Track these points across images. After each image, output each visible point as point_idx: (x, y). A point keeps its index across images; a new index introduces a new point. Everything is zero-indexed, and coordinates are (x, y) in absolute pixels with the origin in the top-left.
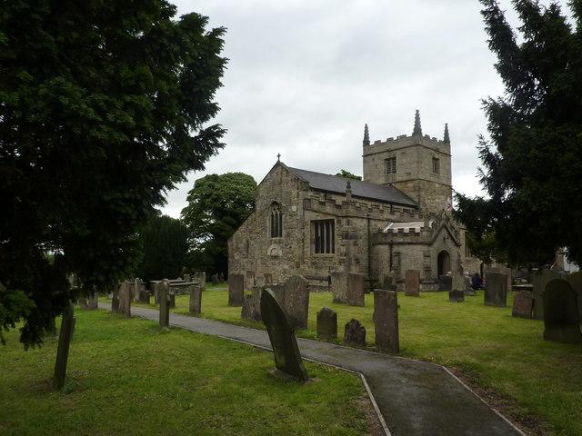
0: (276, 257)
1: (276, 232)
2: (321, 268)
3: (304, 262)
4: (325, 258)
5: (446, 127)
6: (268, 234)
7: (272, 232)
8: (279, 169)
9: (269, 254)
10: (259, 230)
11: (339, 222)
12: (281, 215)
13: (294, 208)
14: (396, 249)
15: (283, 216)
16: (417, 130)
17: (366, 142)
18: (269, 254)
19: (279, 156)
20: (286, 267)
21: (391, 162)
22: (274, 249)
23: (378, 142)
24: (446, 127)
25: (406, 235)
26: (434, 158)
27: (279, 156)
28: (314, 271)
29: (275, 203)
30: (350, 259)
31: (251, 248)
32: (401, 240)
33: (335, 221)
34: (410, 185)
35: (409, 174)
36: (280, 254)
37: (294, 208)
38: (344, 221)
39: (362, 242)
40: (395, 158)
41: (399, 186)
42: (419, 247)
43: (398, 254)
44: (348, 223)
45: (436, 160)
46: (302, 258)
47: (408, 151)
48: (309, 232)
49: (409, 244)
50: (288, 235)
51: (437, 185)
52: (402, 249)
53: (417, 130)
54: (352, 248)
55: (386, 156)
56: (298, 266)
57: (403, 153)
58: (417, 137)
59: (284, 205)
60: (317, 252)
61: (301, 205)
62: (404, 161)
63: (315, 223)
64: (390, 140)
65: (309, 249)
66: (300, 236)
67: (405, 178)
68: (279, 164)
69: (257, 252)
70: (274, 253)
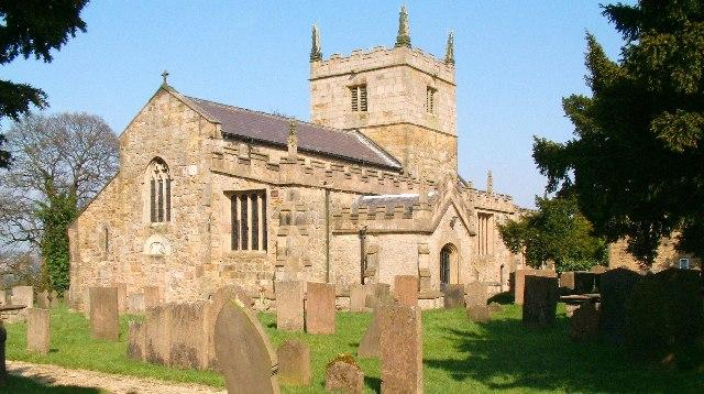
1: (159, 212)
2: (243, 276)
11: (274, 194)
12: (169, 181)
13: (193, 170)
18: (146, 252)
20: (180, 276)
22: (153, 245)
29: (160, 161)
31: (113, 243)
36: (168, 250)
38: (284, 192)
40: (364, 86)
46: (208, 260)
48: (224, 211)
55: (347, 81)
56: (200, 272)
57: (380, 78)
60: (235, 247)
69: (125, 250)
70: (156, 250)
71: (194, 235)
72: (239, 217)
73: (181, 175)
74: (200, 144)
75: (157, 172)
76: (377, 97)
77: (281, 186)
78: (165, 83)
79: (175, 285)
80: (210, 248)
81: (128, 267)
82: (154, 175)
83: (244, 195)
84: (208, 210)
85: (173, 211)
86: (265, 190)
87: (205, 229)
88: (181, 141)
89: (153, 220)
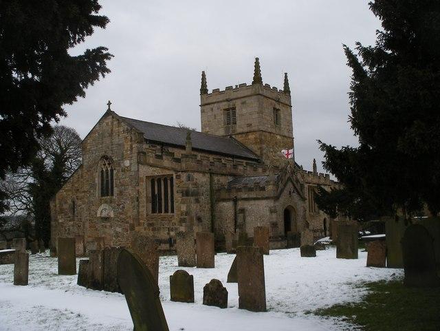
0: (106, 219)
1: (107, 190)
2: (159, 229)
3: (139, 225)
4: (163, 219)
5: (286, 77)
6: (98, 193)
8: (109, 120)
9: (99, 212)
10: (86, 188)
11: (178, 177)
13: (127, 163)
14: (240, 205)
15: (115, 172)
16: (257, 78)
17: (204, 90)
19: (109, 104)
20: (119, 230)
21: (230, 113)
22: (104, 210)
23: (216, 91)
24: (286, 77)
26: (274, 109)
27: (109, 104)
28: (151, 233)
30: (191, 219)
31: (78, 210)
32: (246, 196)
33: (174, 177)
34: (251, 137)
35: (249, 125)
37: (127, 163)
38: (184, 176)
39: (204, 199)
40: (234, 109)
41: (239, 138)
42: (264, 202)
43: (243, 211)
44: (189, 178)
45: (276, 110)
46: (137, 219)
47: (248, 100)
48: (144, 190)
49: (255, 199)
50: (121, 193)
51: (278, 137)
53: (257, 78)
54: (194, 206)
55: (225, 105)
56: (132, 228)
57: (243, 103)
58: (257, 86)
60: (154, 211)
61: (135, 159)
62: (244, 111)
63: (153, 180)
64: (229, 88)
65: (145, 208)
66: (134, 194)
67: (246, 130)
68: (109, 113)
70: (104, 214)
72: (105, 182)
73: (119, 165)
74: (131, 146)
75: (105, 165)
76: (242, 115)
78: (109, 110)
79: (117, 235)
80: (138, 212)
81: (87, 225)
82: (103, 166)
84: (137, 188)
85: (115, 189)
87: (135, 200)
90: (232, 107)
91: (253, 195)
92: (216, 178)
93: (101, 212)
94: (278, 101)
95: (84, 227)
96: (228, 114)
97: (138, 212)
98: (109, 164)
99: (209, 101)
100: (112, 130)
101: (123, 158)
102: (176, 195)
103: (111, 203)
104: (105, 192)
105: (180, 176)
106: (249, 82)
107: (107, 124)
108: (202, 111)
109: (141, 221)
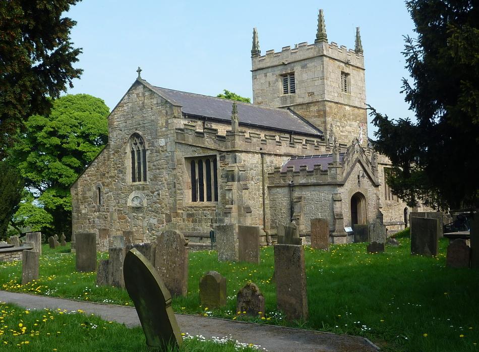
0: (137, 209)
3: (177, 215)
5: (358, 33)
7: (133, 173)
8: (140, 89)
10: (113, 172)
12: (144, 151)
14: (297, 194)
15: (148, 153)
16: (321, 37)
17: (255, 53)
19: (139, 71)
20: (154, 221)
21: (288, 79)
23: (270, 53)
24: (358, 33)
25: (310, 173)
26: (343, 73)
27: (139, 71)
28: (191, 225)
29: (136, 135)
33: (218, 158)
37: (162, 142)
40: (292, 74)
46: (174, 209)
49: (315, 185)
51: (347, 108)
52: (307, 193)
53: (321, 37)
59: (147, 137)
62: (305, 76)
63: (192, 161)
64: (286, 49)
67: (307, 100)
68: (138, 83)
70: (136, 203)
71: (164, 192)
75: (136, 144)
77: (227, 152)
80: (175, 200)
81: (116, 216)
82: (134, 146)
83: (200, 160)
84: (174, 172)
86: (216, 155)
88: (153, 121)
89: (134, 180)
90: (289, 72)
91: (312, 180)
92: (268, 159)
93: (133, 200)
94: (347, 63)
95: (112, 219)
96: (285, 82)
97: (175, 200)
98: (141, 143)
99: (261, 65)
100: (143, 103)
101: (157, 137)
102: (220, 180)
103: (143, 190)
104: (137, 176)
105: (224, 157)
106: (311, 39)
107: (138, 94)
108: (254, 78)
109: (179, 211)
